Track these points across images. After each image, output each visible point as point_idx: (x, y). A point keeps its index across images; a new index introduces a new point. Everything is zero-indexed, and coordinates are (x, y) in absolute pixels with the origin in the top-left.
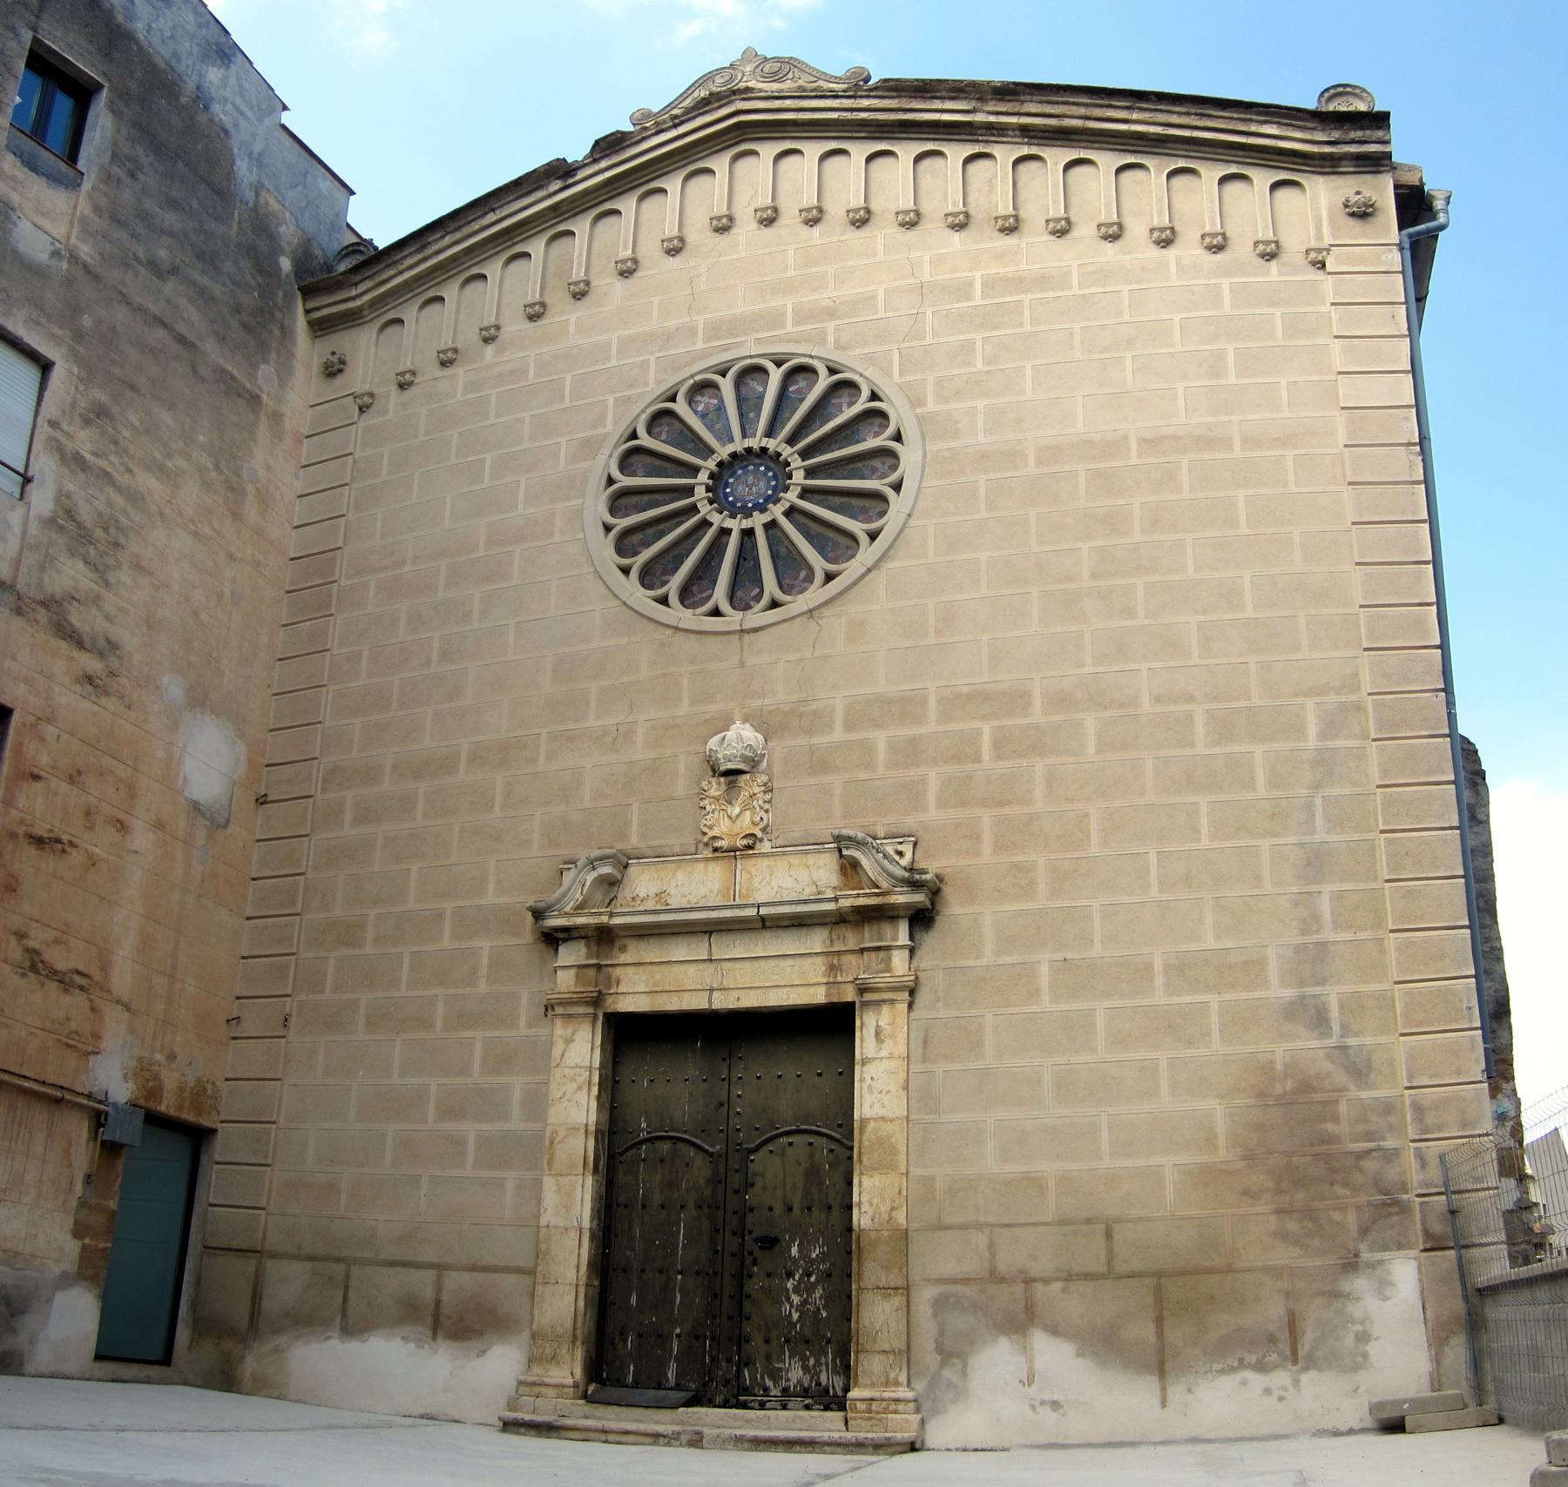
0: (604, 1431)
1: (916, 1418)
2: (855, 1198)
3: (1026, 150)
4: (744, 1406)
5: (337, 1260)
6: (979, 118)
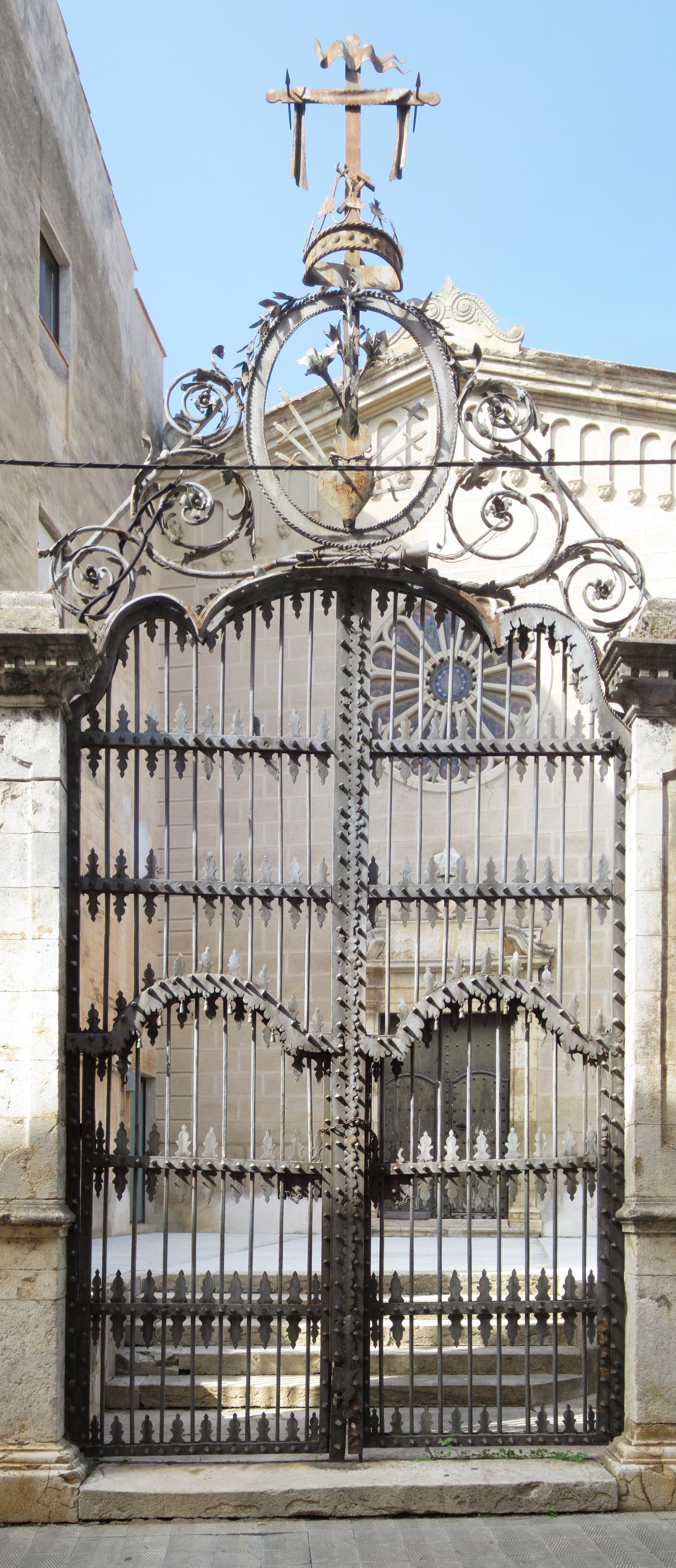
0: (401, 1231)
1: (540, 1222)
2: (511, 1106)
3: (618, 425)
4: (454, 1217)
5: (238, 1144)
6: (596, 394)
